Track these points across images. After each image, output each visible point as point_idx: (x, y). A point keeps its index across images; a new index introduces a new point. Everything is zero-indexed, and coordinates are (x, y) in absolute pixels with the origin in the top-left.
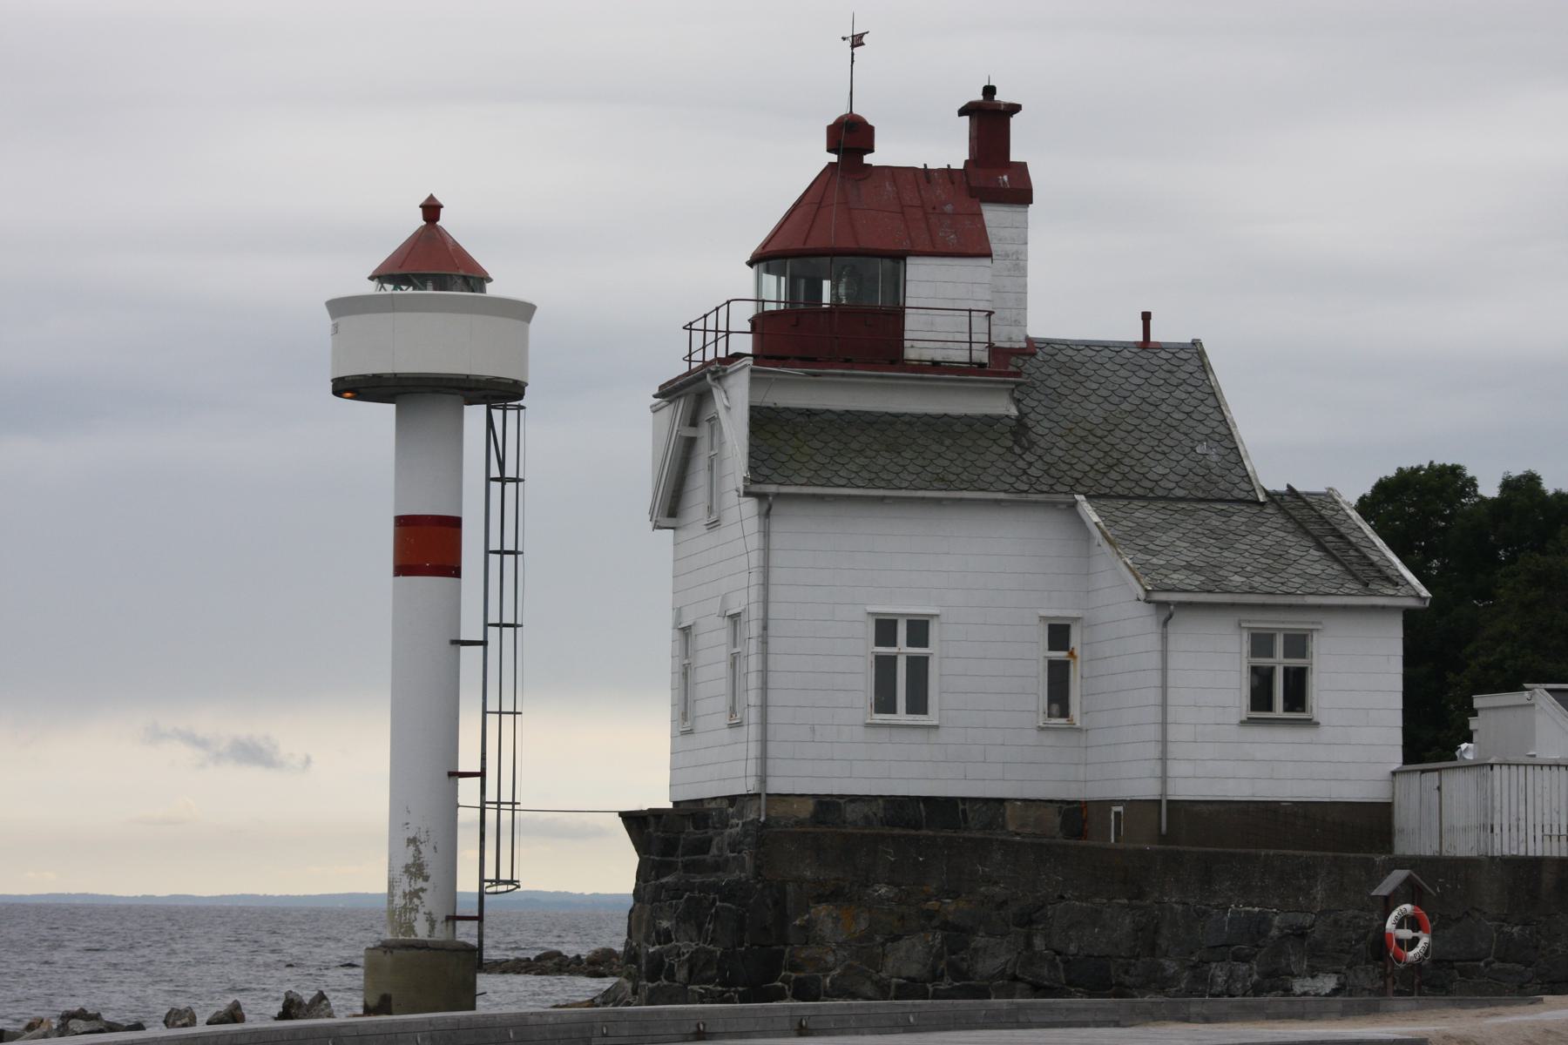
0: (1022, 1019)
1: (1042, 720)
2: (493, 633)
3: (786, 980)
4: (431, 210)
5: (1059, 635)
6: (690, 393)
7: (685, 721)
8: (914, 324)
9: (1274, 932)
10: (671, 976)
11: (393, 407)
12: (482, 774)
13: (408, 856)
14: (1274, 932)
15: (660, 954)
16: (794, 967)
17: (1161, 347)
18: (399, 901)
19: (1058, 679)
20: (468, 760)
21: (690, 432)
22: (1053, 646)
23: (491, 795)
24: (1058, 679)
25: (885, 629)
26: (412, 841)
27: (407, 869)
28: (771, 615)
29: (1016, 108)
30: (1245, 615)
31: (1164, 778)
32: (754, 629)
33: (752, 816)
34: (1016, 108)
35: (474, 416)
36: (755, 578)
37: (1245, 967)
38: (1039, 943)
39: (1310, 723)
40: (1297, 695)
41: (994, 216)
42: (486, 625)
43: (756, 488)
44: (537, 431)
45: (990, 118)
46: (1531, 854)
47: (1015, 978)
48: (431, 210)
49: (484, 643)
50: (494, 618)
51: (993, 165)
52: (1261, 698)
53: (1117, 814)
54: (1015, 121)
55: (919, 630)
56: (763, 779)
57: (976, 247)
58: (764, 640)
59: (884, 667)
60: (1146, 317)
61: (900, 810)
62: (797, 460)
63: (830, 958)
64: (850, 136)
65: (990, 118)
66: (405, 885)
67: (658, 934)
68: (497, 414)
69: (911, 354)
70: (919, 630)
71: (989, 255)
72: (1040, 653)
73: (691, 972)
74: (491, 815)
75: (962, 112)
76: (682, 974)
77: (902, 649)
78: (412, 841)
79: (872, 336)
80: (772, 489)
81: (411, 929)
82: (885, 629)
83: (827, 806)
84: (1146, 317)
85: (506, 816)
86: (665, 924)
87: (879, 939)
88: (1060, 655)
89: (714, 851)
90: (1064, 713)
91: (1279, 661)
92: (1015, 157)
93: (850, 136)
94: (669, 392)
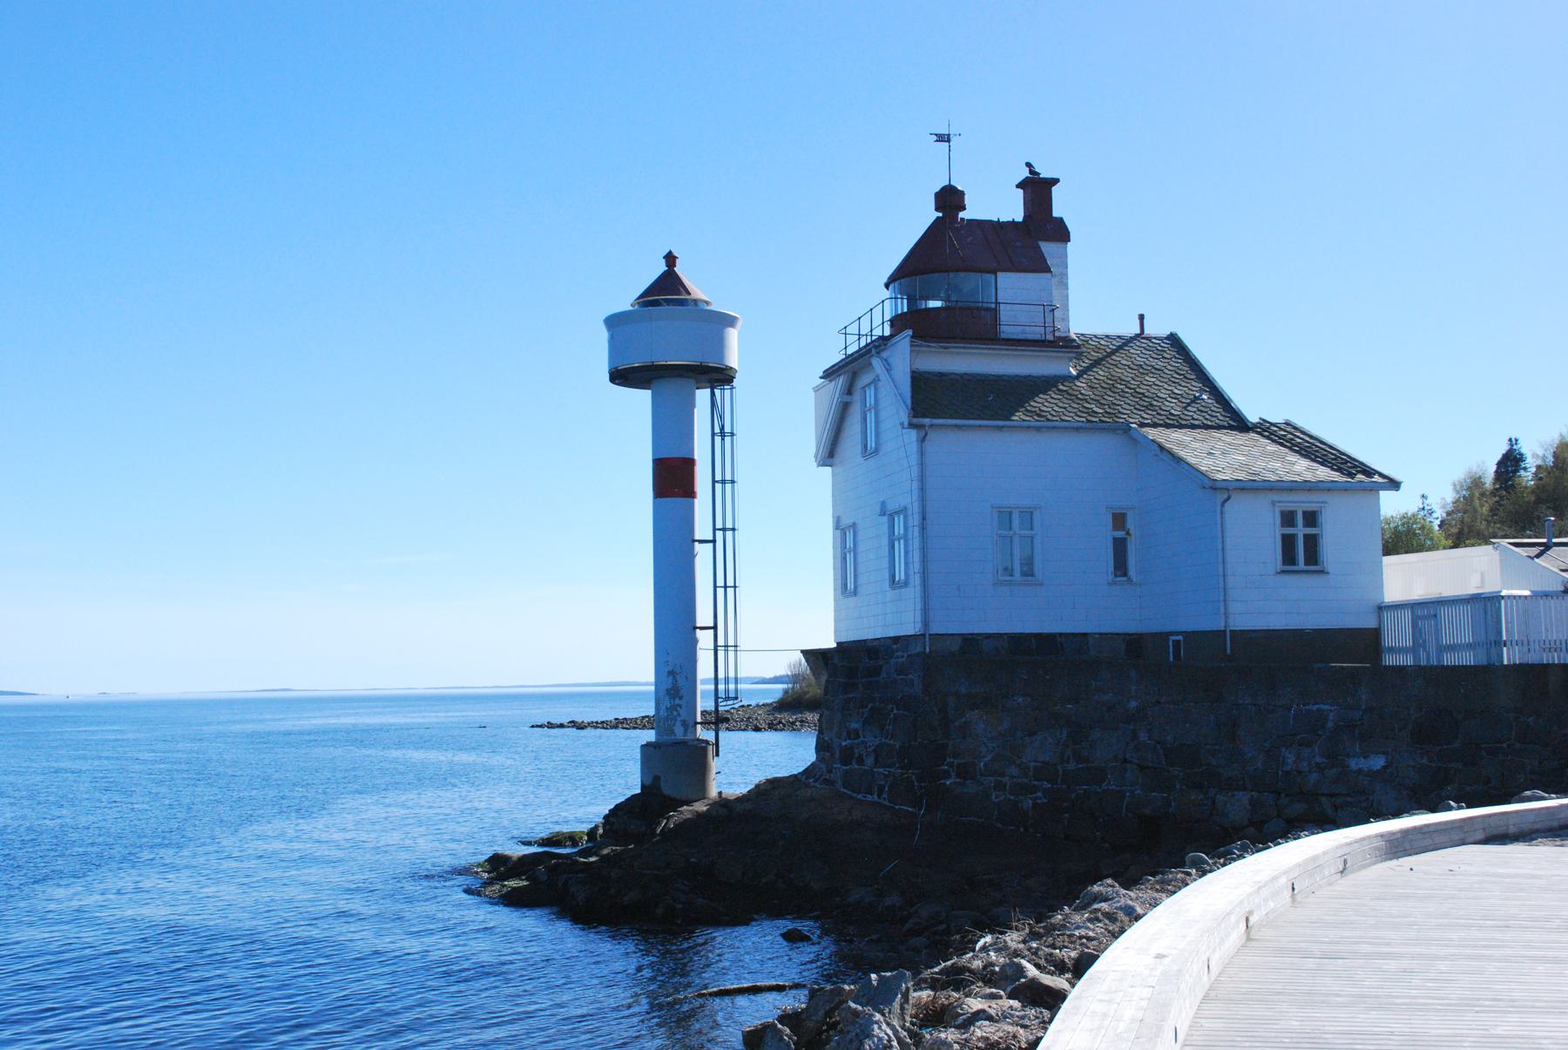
0: (1407, 846)
1: (1111, 577)
2: (719, 534)
3: (951, 765)
4: (670, 259)
5: (1119, 520)
6: (849, 372)
7: (847, 588)
8: (1005, 314)
9: (1330, 724)
10: (861, 761)
11: (648, 393)
12: (715, 628)
13: (668, 683)
14: (1330, 724)
15: (852, 747)
16: (956, 755)
17: (1149, 339)
18: (663, 713)
19: (1120, 548)
20: (703, 616)
21: (847, 398)
22: (1116, 528)
23: (721, 642)
24: (1120, 548)
25: (1005, 516)
26: (671, 673)
27: (668, 692)
28: (928, 509)
29: (1056, 181)
30: (1275, 497)
31: (1226, 615)
32: (915, 520)
33: (919, 649)
34: (1056, 181)
35: (702, 396)
36: (915, 485)
37: (1307, 751)
38: (1143, 736)
39: (1322, 572)
40: (1313, 556)
41: (1047, 248)
42: (715, 529)
43: (916, 421)
44: (743, 397)
45: (1037, 189)
46: (1423, 663)
47: (1125, 761)
48: (670, 259)
49: (714, 541)
50: (719, 525)
51: (1037, 231)
52: (1289, 556)
53: (1177, 643)
54: (1054, 189)
55: (1028, 515)
56: (926, 623)
57: (1040, 265)
58: (923, 528)
59: (1288, 543)
60: (1141, 317)
61: (1019, 643)
62: (933, 400)
63: (984, 749)
64: (949, 199)
65: (1037, 189)
66: (667, 703)
67: (849, 733)
68: (717, 392)
69: (1007, 331)
70: (1028, 515)
71: (1048, 270)
72: (1105, 534)
73: (876, 760)
74: (721, 654)
75: (1018, 186)
76: (870, 761)
77: (1300, 530)
78: (671, 673)
79: (977, 325)
80: (927, 421)
81: (672, 732)
82: (1005, 516)
83: (970, 642)
84: (1141, 317)
85: (731, 654)
86: (854, 726)
87: (1019, 734)
88: (1121, 534)
89: (884, 675)
90: (1125, 574)
91: (1300, 530)
92: (1056, 214)
93: (949, 199)
94: (829, 374)
